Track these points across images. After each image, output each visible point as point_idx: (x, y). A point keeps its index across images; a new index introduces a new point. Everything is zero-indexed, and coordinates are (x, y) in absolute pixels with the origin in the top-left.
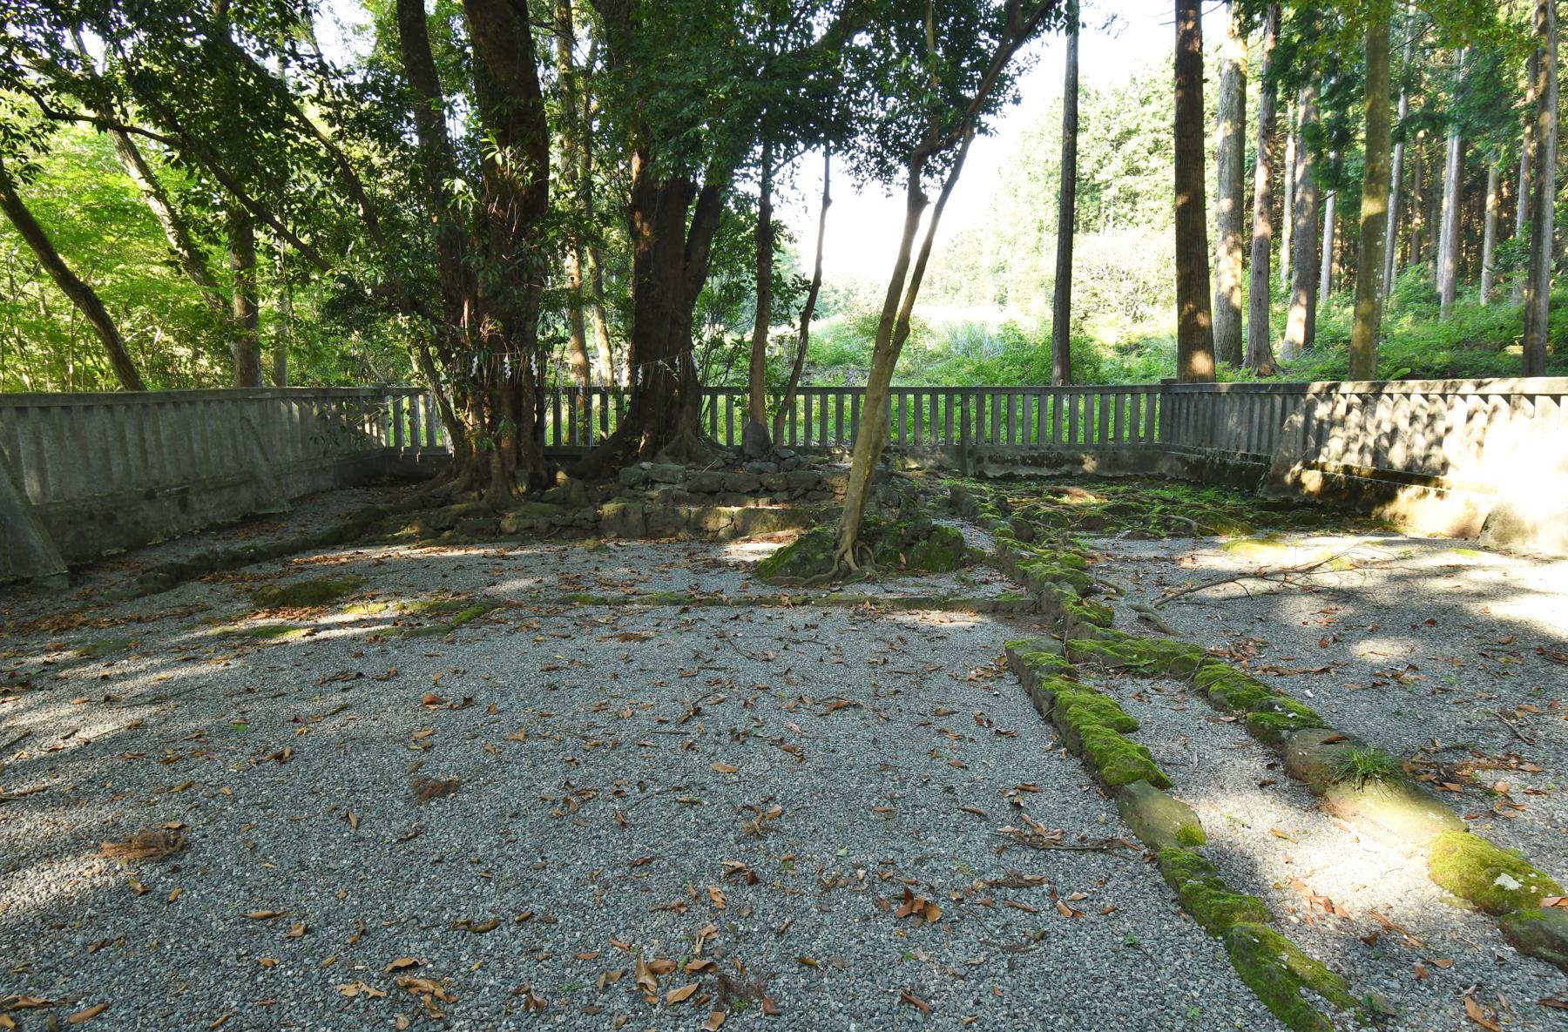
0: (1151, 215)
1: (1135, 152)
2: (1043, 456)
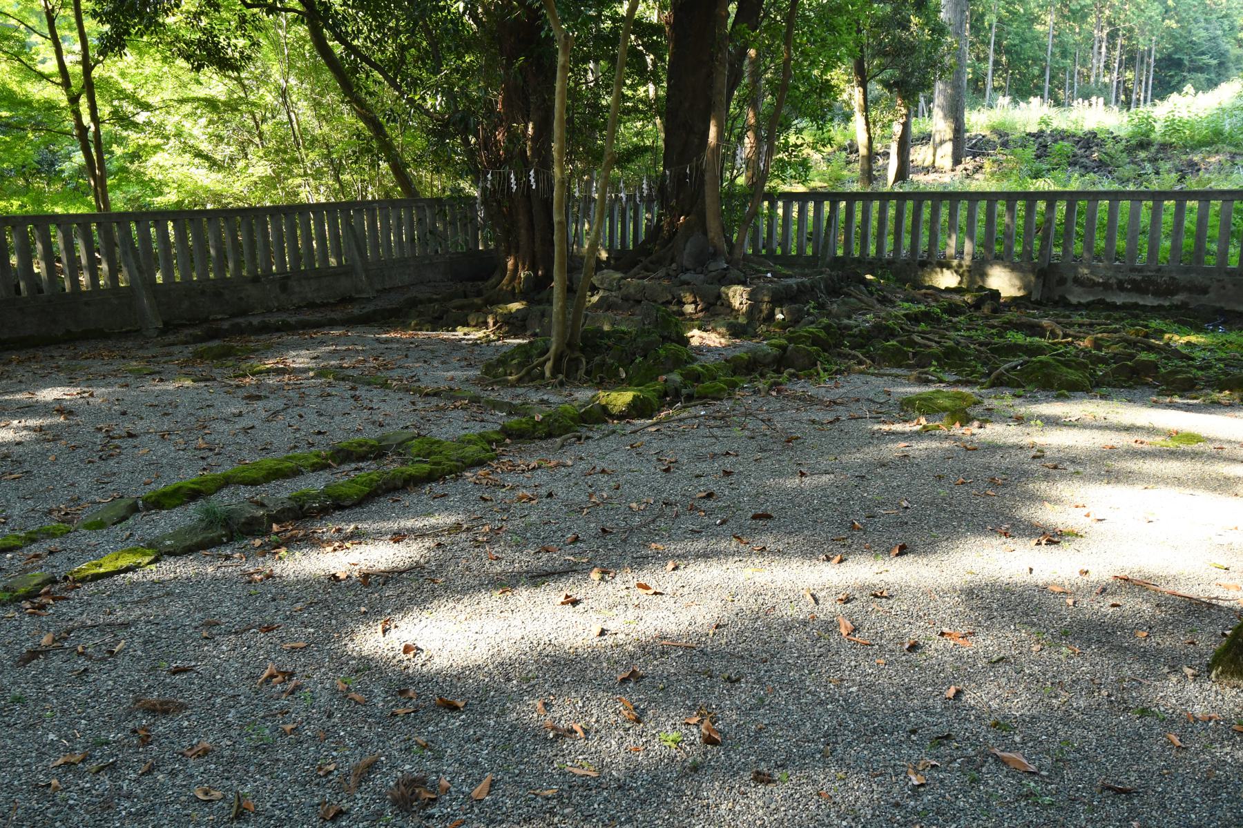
2: (1149, 281)
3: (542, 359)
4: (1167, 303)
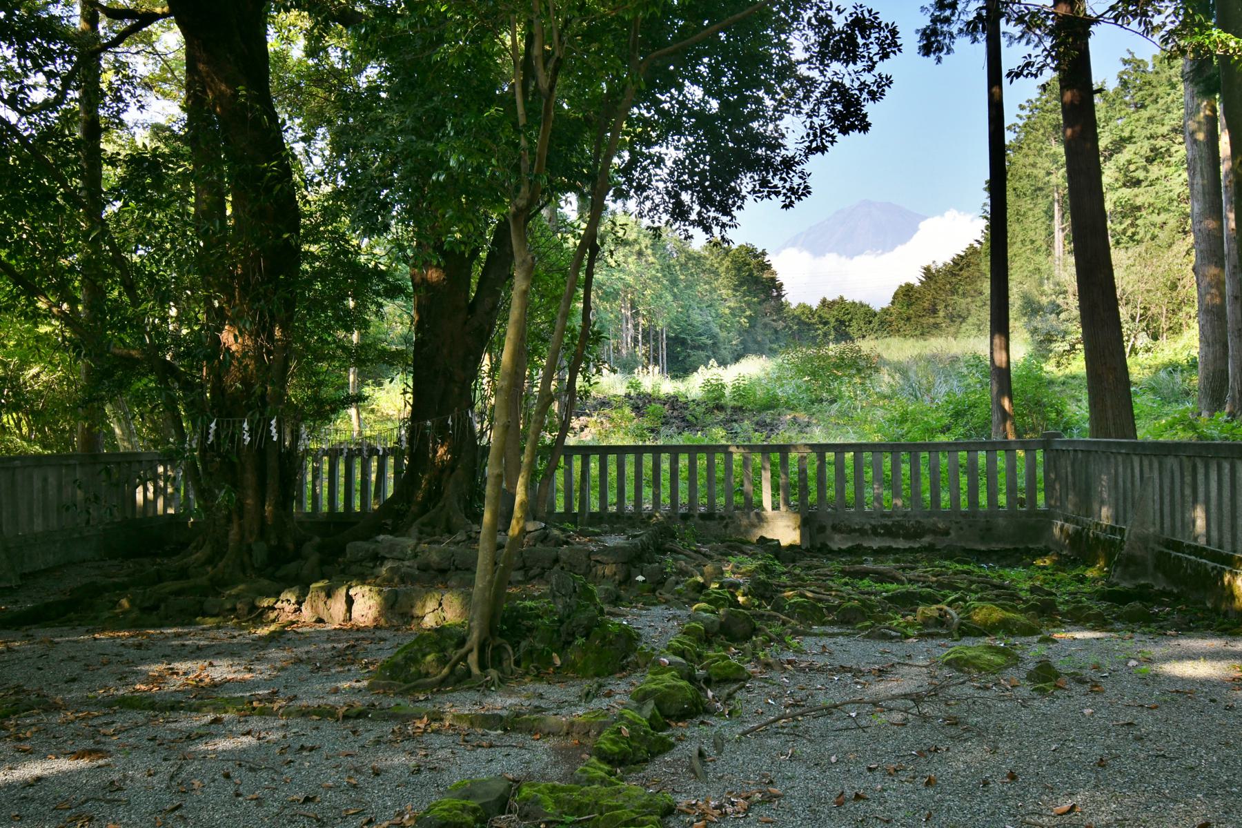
0: (1157, 231)
1: (1130, 162)
2: (900, 526)
3: (463, 651)
4: (917, 545)
